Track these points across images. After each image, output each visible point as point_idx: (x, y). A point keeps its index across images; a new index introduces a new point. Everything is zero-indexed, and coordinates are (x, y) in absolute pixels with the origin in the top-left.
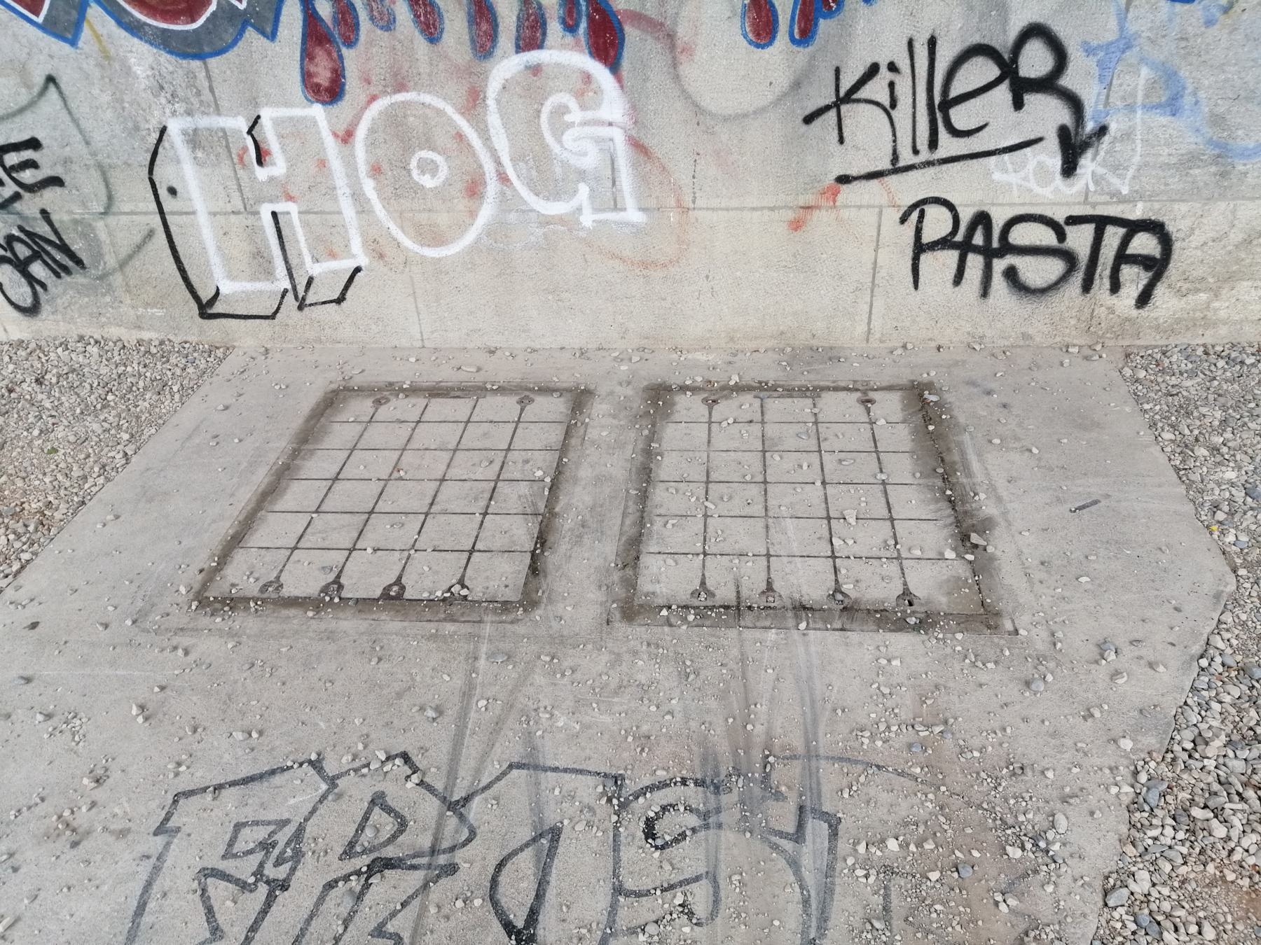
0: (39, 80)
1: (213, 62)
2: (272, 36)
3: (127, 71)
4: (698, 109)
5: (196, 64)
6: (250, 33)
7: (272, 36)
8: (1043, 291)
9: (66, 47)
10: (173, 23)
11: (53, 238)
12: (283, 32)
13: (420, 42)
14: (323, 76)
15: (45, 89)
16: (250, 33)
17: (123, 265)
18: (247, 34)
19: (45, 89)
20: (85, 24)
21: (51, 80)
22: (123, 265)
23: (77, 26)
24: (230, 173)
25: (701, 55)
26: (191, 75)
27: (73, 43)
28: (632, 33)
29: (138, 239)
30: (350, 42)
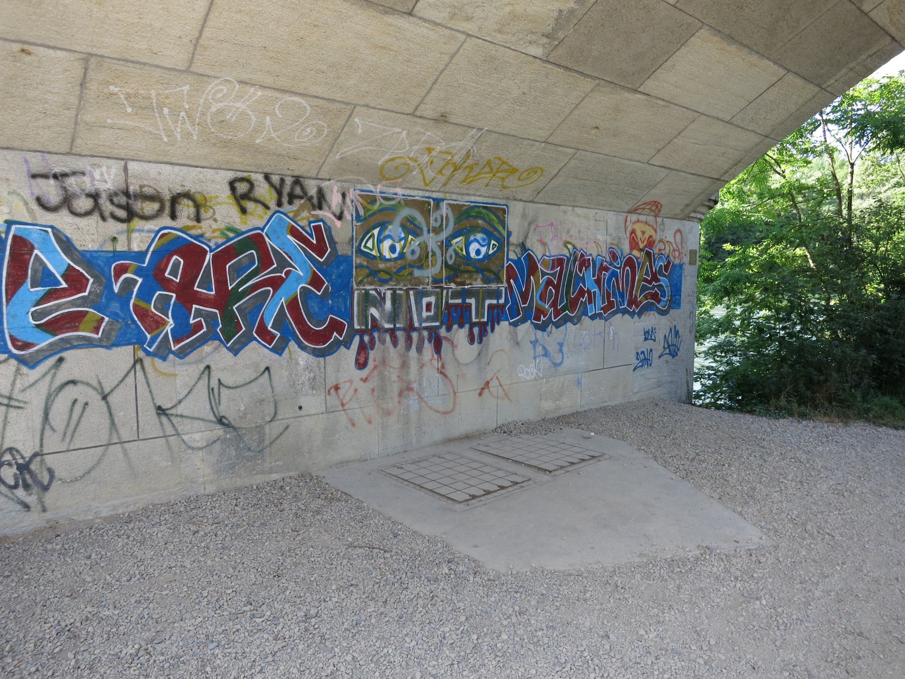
0: (263, 369)
1: (327, 358)
2: (348, 348)
3: (297, 363)
4: (459, 363)
5: (321, 359)
6: (342, 347)
7: (348, 348)
8: (453, 410)
9: (277, 356)
10: (358, 320)
11: (48, 378)
12: (352, 346)
13: (391, 346)
14: (362, 361)
15: (264, 372)
16: (342, 347)
17: (271, 443)
18: (811, 86)
19: (264, 372)
20: (287, 350)
21: (267, 369)
22: (271, 443)
23: (283, 349)
24: (323, 397)
25: (459, 347)
26: (319, 363)
27: (280, 354)
28: (444, 342)
29: (281, 430)
30: (372, 349)
